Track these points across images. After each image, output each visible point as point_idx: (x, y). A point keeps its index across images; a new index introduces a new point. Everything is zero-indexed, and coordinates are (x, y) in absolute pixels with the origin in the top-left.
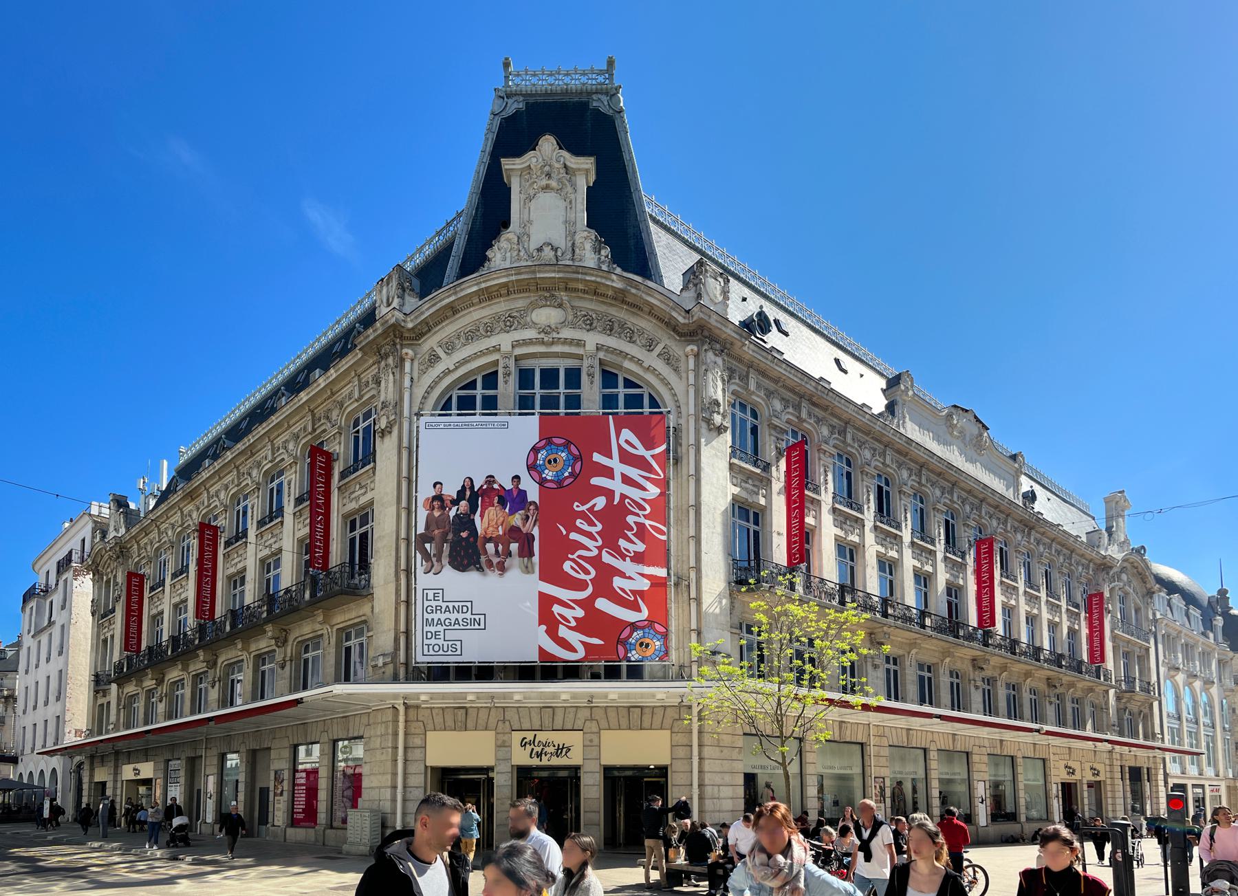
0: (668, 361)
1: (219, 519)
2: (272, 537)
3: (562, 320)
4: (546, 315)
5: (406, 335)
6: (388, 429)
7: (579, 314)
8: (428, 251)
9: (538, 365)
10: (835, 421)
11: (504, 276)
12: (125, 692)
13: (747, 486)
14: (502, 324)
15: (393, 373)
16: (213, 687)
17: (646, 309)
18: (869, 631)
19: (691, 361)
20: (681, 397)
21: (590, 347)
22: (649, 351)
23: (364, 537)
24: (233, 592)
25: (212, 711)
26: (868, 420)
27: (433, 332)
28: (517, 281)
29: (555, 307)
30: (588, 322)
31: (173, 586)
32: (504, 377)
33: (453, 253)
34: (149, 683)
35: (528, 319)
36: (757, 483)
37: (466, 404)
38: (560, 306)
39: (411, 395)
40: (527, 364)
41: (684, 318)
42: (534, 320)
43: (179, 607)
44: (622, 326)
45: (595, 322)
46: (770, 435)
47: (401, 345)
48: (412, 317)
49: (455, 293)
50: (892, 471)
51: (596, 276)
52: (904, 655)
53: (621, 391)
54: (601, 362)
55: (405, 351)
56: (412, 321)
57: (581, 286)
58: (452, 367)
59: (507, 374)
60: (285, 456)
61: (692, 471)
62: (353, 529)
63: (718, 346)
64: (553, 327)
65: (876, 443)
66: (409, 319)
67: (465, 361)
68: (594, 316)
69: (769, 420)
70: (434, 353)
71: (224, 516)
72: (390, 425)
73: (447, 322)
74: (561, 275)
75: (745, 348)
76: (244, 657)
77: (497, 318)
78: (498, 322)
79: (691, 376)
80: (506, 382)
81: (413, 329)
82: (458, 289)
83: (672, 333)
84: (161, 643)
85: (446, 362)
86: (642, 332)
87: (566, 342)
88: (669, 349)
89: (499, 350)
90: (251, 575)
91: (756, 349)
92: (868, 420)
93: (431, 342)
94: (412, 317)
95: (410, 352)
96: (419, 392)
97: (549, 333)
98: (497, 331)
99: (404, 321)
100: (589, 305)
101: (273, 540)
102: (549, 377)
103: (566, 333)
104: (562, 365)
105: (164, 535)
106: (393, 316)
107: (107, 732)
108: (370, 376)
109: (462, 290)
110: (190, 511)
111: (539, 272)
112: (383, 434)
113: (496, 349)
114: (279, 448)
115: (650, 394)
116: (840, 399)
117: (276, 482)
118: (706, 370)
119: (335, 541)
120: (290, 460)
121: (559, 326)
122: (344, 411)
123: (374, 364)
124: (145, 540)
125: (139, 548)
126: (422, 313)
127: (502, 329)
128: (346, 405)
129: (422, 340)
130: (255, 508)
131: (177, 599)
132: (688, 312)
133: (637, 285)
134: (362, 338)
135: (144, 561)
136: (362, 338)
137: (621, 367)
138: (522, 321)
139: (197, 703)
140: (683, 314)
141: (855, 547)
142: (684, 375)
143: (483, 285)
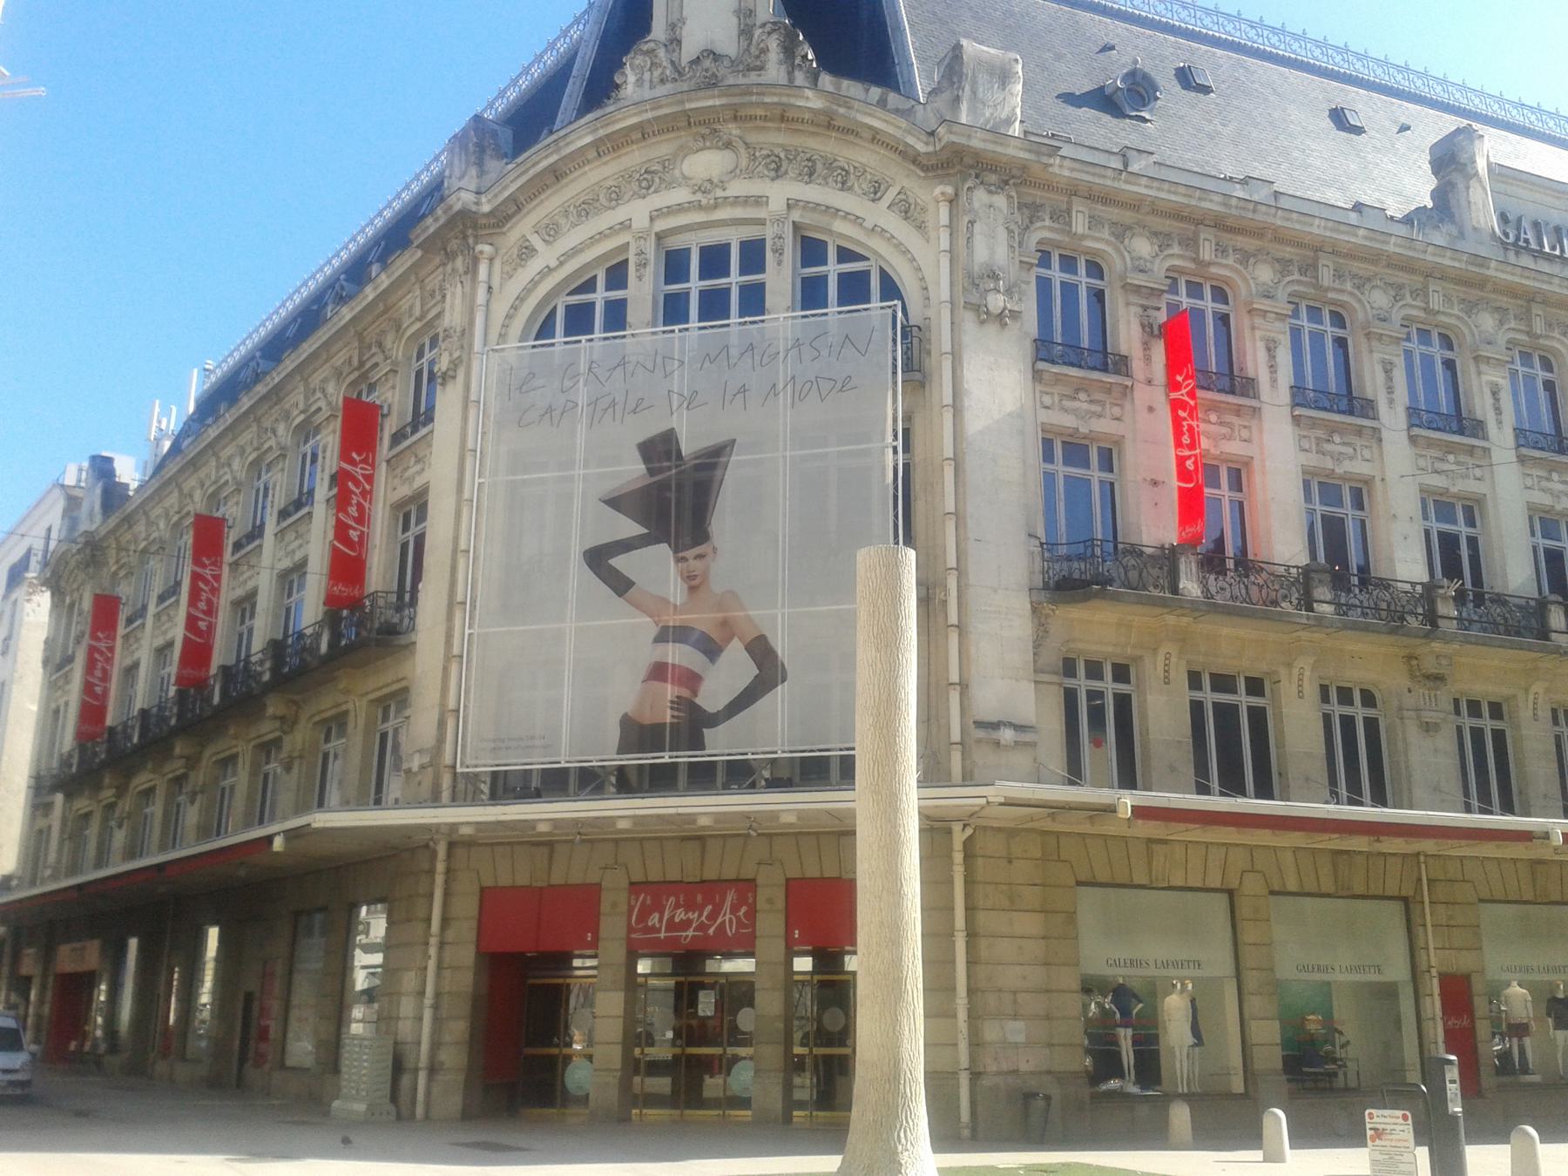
0: (906, 214)
1: (229, 504)
2: (296, 538)
3: (731, 167)
4: (706, 163)
5: (483, 221)
6: (451, 373)
7: (757, 154)
8: (550, 60)
9: (694, 242)
10: (1288, 252)
11: (635, 114)
12: (74, 808)
13: (1076, 404)
14: (635, 186)
15: (462, 282)
16: (192, 802)
17: (867, 134)
18: (1407, 651)
19: (944, 211)
20: (928, 272)
21: (777, 205)
22: (873, 201)
23: (420, 541)
24: (238, 629)
25: (190, 846)
26: (1366, 238)
27: (525, 211)
28: (656, 119)
29: (718, 148)
30: (773, 166)
31: (280, 535)
32: (637, 270)
33: (574, 72)
34: (108, 794)
35: (677, 172)
36: (1097, 396)
37: (579, 320)
38: (728, 145)
39: (487, 319)
40: (676, 243)
41: (927, 144)
42: (686, 173)
43: (291, 577)
44: (830, 165)
45: (785, 164)
46: (1128, 304)
47: (476, 237)
48: (490, 197)
49: (558, 150)
50: (1453, 321)
51: (781, 95)
52: (1514, 696)
53: (833, 269)
54: (796, 227)
55: (479, 247)
56: (489, 201)
57: (760, 112)
58: (553, 264)
59: (642, 265)
60: (322, 404)
61: (948, 399)
62: (406, 528)
63: (993, 178)
64: (715, 181)
65: (1401, 274)
66: (484, 199)
67: (575, 251)
68: (782, 155)
69: (1123, 277)
70: (527, 244)
71: (280, 467)
72: (455, 364)
73: (549, 192)
74: (723, 101)
75: (1056, 170)
76: (239, 749)
77: (627, 176)
78: (630, 182)
79: (944, 237)
80: (640, 278)
81: (491, 212)
82: (561, 144)
83: (912, 167)
84: (248, 656)
85: (546, 256)
86: (862, 171)
87: (737, 201)
88: (908, 193)
89: (630, 226)
90: (264, 602)
91: (1077, 166)
92: (1366, 238)
93: (523, 228)
94: (490, 197)
95: (487, 249)
96: (500, 308)
97: (709, 192)
98: (626, 197)
99: (477, 204)
100: (775, 139)
101: (296, 543)
102: (714, 260)
103: (737, 188)
104: (734, 238)
105: (319, 395)
106: (459, 199)
107: (43, 882)
108: (436, 281)
109: (568, 144)
110: (193, 488)
111: (690, 100)
112: (444, 379)
113: (625, 226)
114: (314, 391)
115: (880, 267)
116: (1287, 215)
117: (311, 442)
118: (972, 222)
119: (377, 551)
120: (325, 413)
121: (725, 179)
122: (403, 333)
123: (438, 268)
124: (128, 536)
125: (120, 549)
126: (505, 188)
127: (634, 193)
128: (405, 325)
129: (509, 225)
130: (278, 488)
131: (286, 563)
132: (932, 134)
133: (846, 102)
134: (419, 231)
135: (122, 573)
136: (419, 231)
137: (830, 232)
138: (667, 177)
139: (170, 836)
140: (924, 137)
141: (1366, 482)
142: (932, 234)
143: (601, 133)
